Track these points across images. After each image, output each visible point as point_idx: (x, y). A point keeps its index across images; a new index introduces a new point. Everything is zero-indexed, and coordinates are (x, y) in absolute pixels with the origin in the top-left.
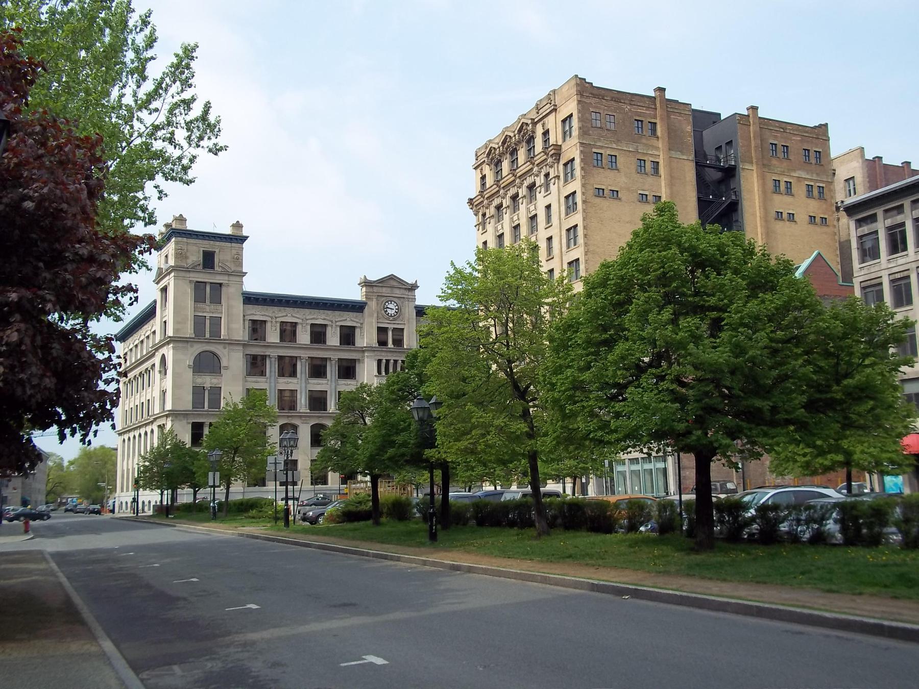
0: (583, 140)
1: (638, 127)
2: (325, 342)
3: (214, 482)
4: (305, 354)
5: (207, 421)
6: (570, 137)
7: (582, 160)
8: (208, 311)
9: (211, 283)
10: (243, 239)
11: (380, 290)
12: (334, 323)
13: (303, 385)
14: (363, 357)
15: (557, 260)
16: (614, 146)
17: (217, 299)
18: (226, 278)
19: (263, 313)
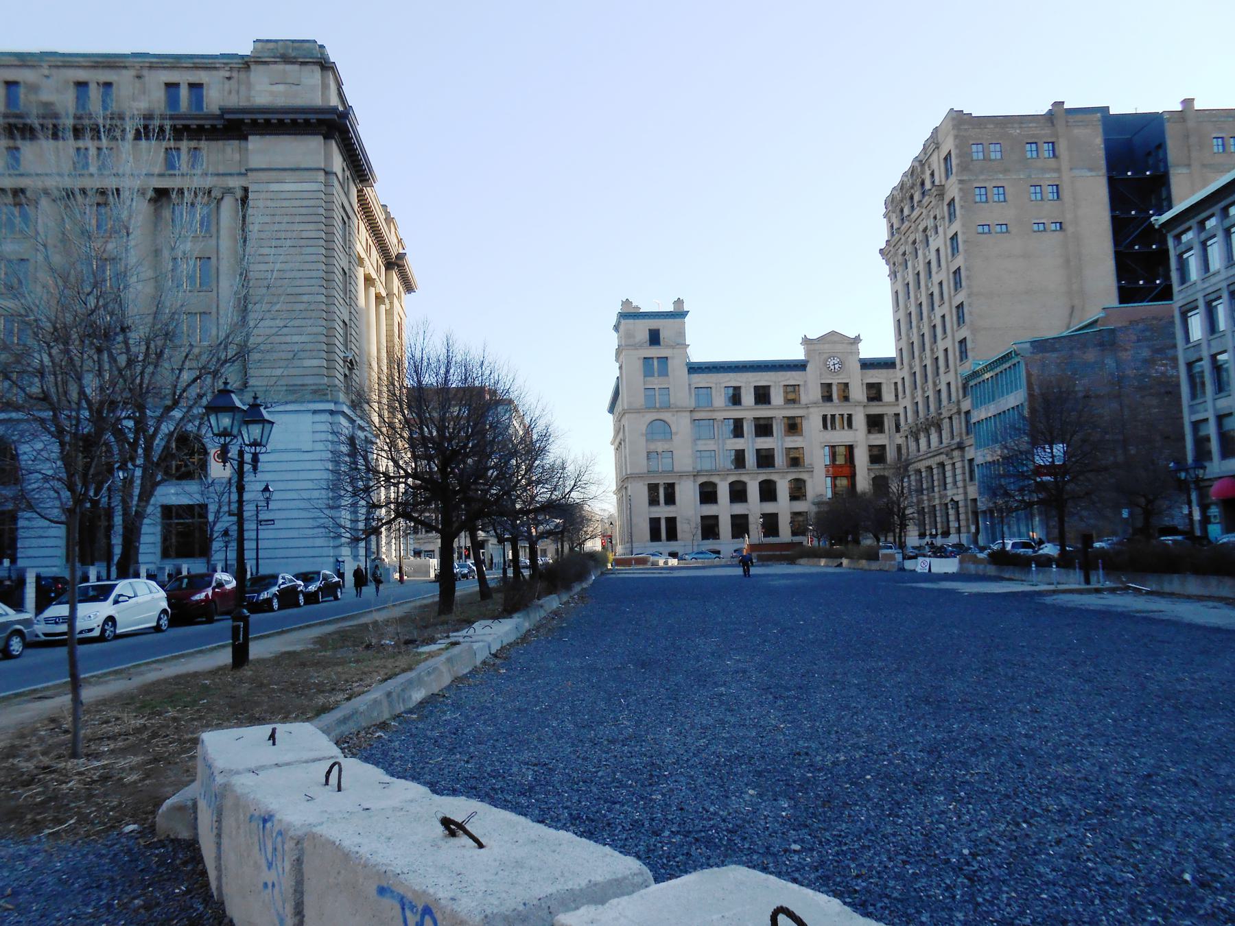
2: (769, 403)
7: (961, 199)
8: (656, 382)
15: (947, 304)
16: (1001, 176)
17: (664, 372)
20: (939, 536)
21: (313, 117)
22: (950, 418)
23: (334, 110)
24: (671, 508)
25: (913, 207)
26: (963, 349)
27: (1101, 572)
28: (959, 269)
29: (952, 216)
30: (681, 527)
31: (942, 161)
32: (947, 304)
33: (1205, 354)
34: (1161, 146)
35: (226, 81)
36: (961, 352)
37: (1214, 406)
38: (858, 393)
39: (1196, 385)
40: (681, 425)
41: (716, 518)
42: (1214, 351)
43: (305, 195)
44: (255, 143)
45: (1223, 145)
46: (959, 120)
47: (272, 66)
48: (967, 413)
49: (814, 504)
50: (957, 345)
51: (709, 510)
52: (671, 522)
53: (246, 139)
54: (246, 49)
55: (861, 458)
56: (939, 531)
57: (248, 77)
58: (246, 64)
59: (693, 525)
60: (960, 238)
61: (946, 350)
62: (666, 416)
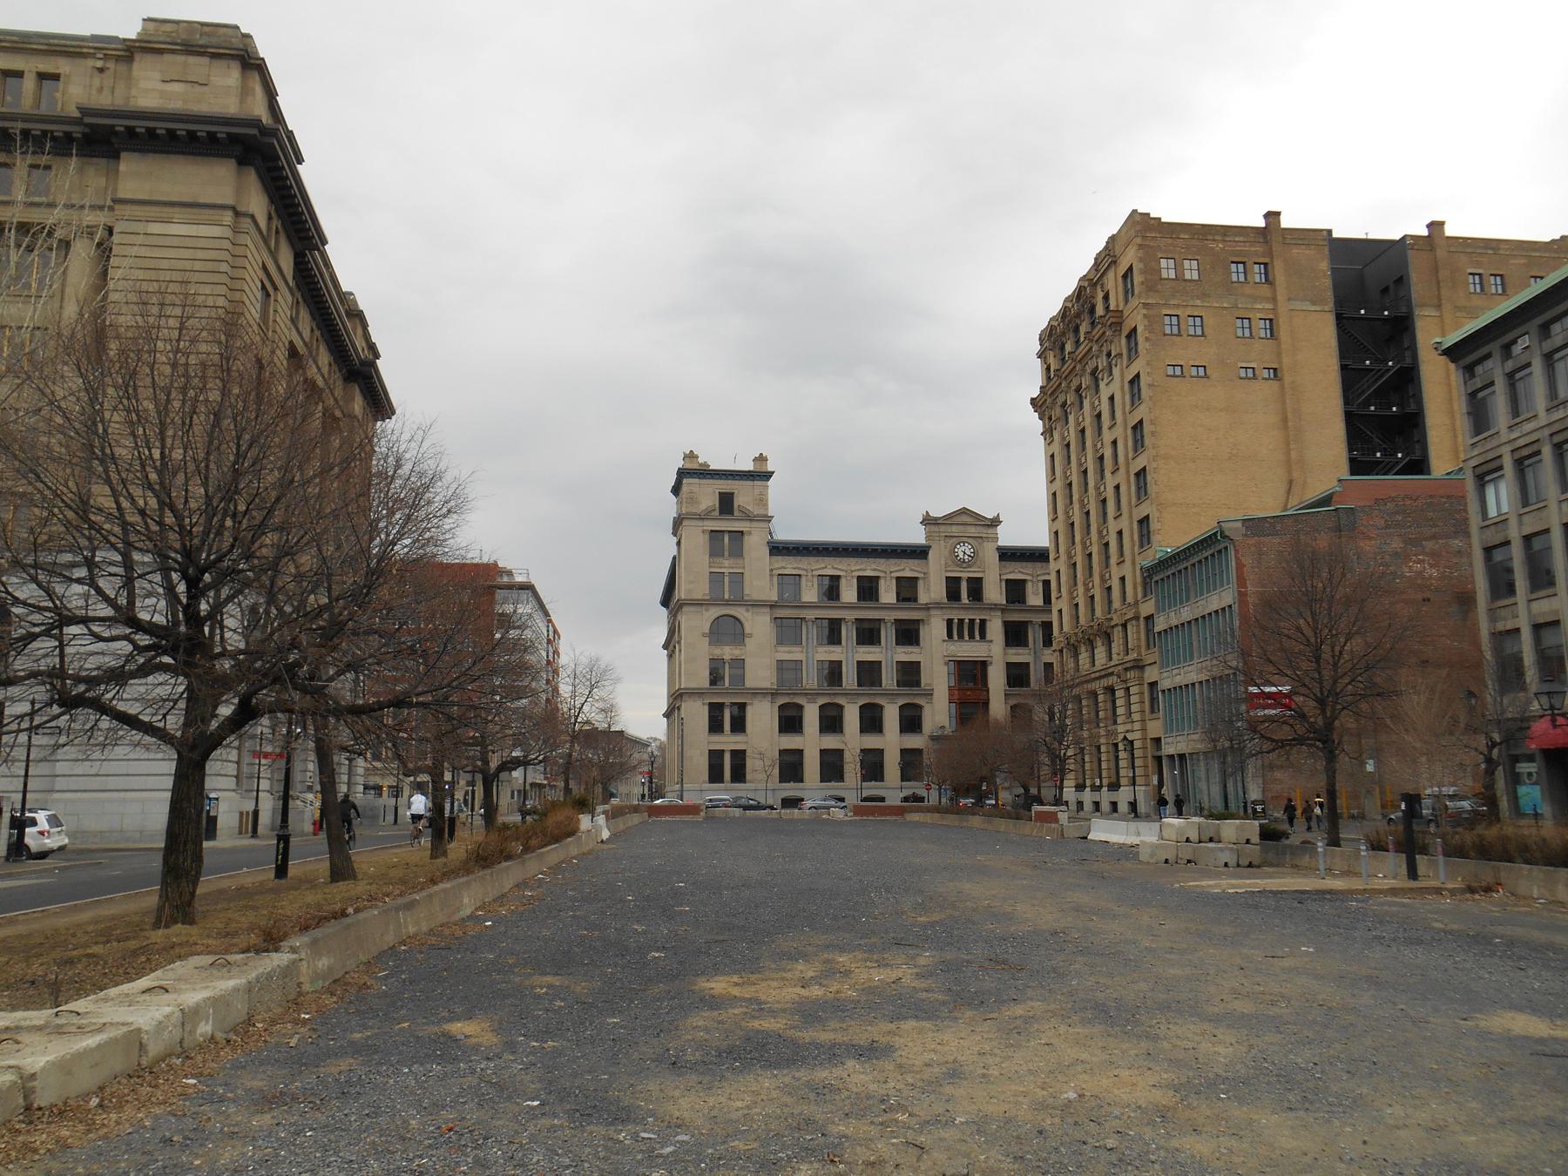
0: (1147, 299)
1: (1496, 285)
3: (18, 776)
4: (850, 615)
5: (727, 700)
6: (1133, 295)
8: (727, 566)
9: (730, 532)
10: (767, 476)
11: (948, 528)
12: (887, 573)
13: (850, 654)
14: (929, 616)
16: (1198, 302)
17: (738, 552)
18: (747, 524)
19: (796, 565)
20: (1105, 789)
21: (222, 131)
22: (1124, 626)
23: (256, 123)
24: (739, 738)
25: (1063, 359)
26: (1145, 532)
27: (1441, 858)
28: (1141, 422)
29: (1133, 351)
30: (751, 764)
31: (1120, 280)
32: (1122, 470)
33: (1514, 533)
34: (1401, 281)
35: (96, 73)
36: (1141, 536)
37: (1529, 612)
38: (994, 593)
39: (1502, 585)
40: (759, 626)
41: (800, 752)
42: (1527, 530)
43: (202, 243)
44: (129, 164)
45: (1481, 284)
46: (1142, 226)
47: (167, 57)
48: (1149, 618)
49: (933, 738)
50: (1135, 525)
51: (791, 741)
52: (739, 757)
53: (117, 157)
54: (129, 29)
55: (997, 679)
56: (1105, 782)
57: (130, 70)
58: (127, 52)
59: (768, 763)
60: (1144, 381)
61: (1120, 533)
62: (739, 612)
